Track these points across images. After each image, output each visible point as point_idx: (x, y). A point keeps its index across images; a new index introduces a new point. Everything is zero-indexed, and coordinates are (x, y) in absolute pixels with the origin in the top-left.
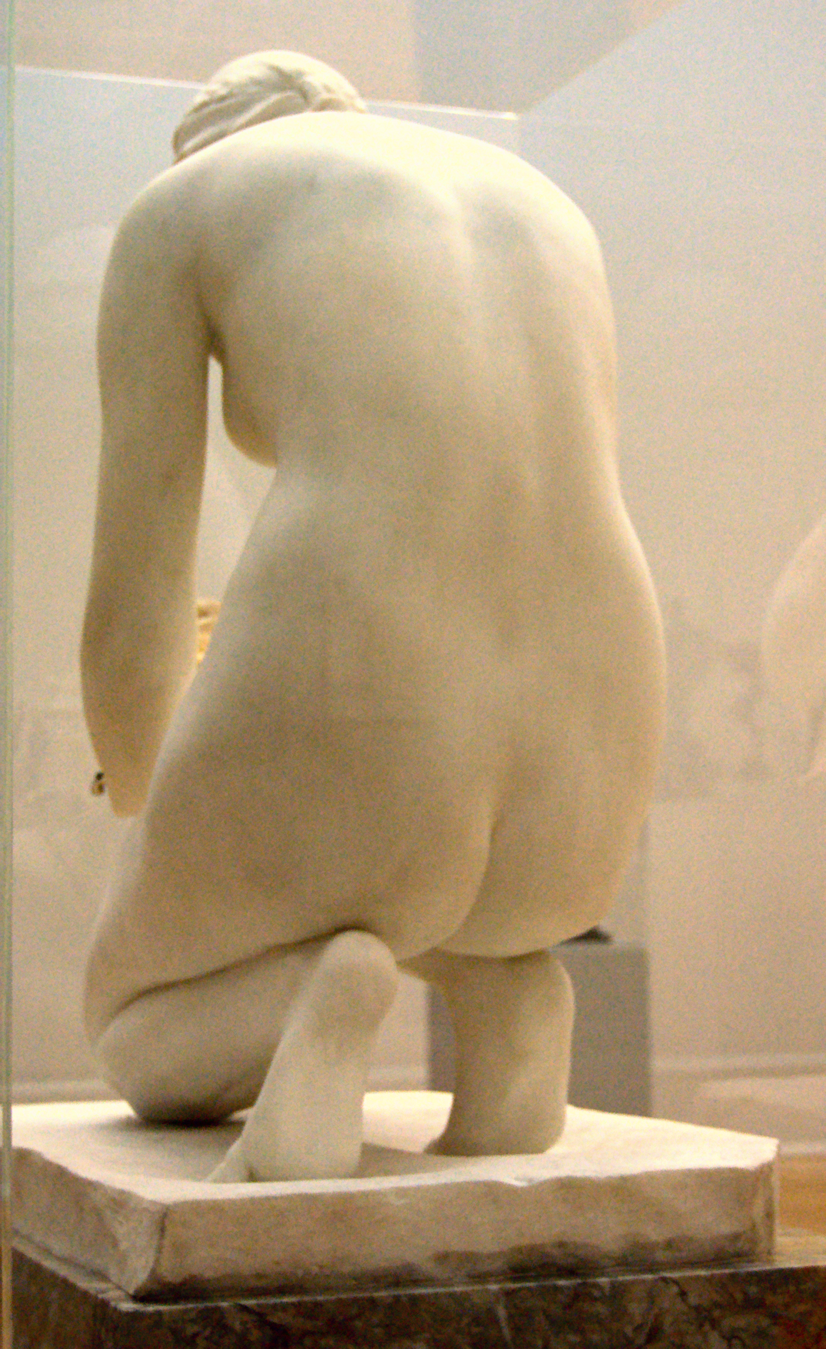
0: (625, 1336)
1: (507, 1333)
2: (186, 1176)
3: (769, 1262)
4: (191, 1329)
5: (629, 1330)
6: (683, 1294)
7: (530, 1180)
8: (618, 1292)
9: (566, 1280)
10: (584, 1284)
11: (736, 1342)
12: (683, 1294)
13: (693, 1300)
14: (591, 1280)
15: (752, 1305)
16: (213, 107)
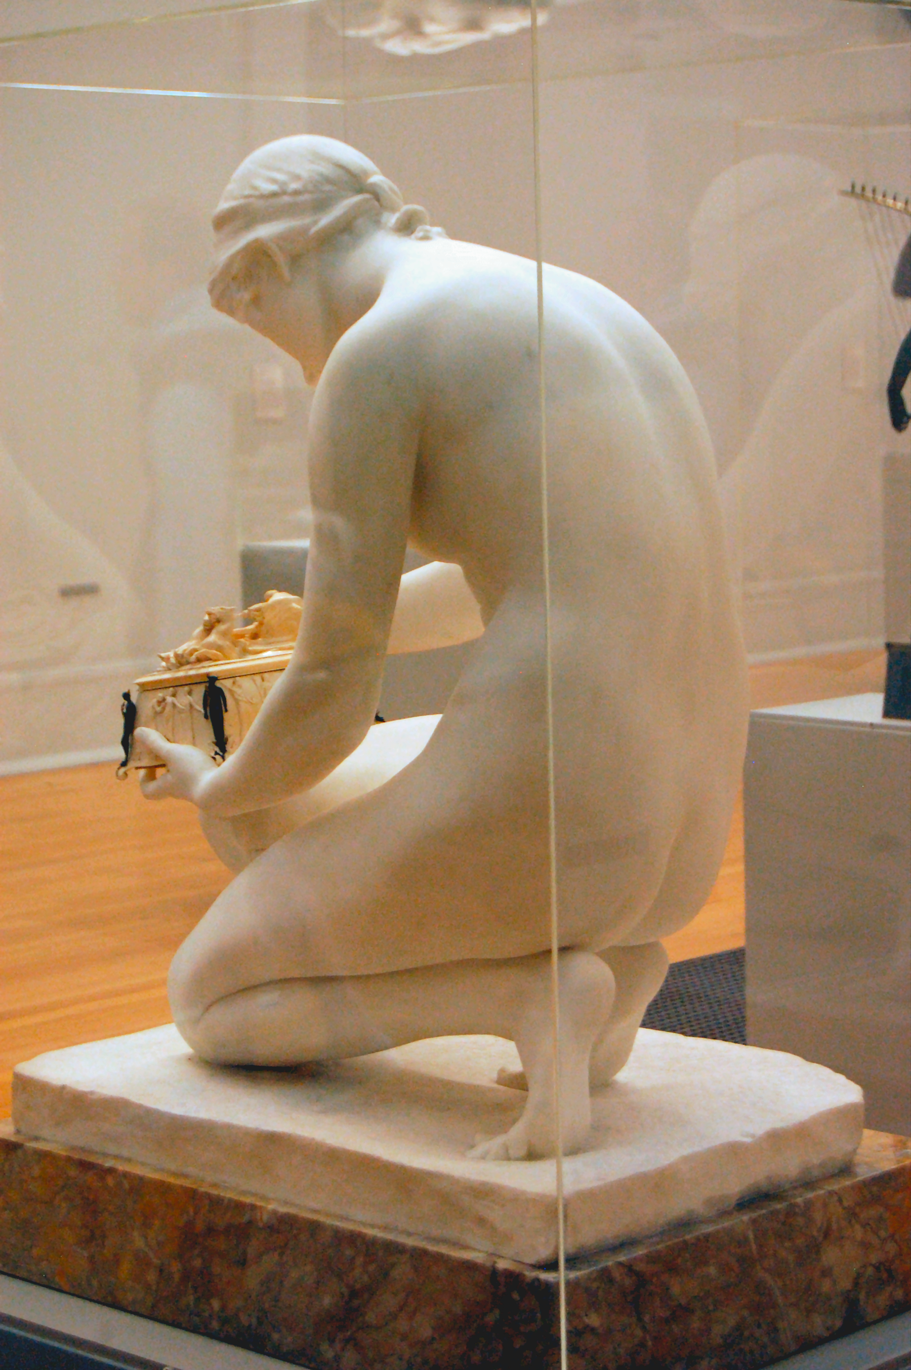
0: (813, 1237)
2: (211, 673)
3: (856, 1175)
4: (595, 1285)
6: (840, 1201)
7: (753, 1136)
9: (859, 1180)
10: (791, 1204)
11: (868, 1228)
12: (840, 1201)
14: (793, 1201)
15: (876, 1200)
16: (286, 199)
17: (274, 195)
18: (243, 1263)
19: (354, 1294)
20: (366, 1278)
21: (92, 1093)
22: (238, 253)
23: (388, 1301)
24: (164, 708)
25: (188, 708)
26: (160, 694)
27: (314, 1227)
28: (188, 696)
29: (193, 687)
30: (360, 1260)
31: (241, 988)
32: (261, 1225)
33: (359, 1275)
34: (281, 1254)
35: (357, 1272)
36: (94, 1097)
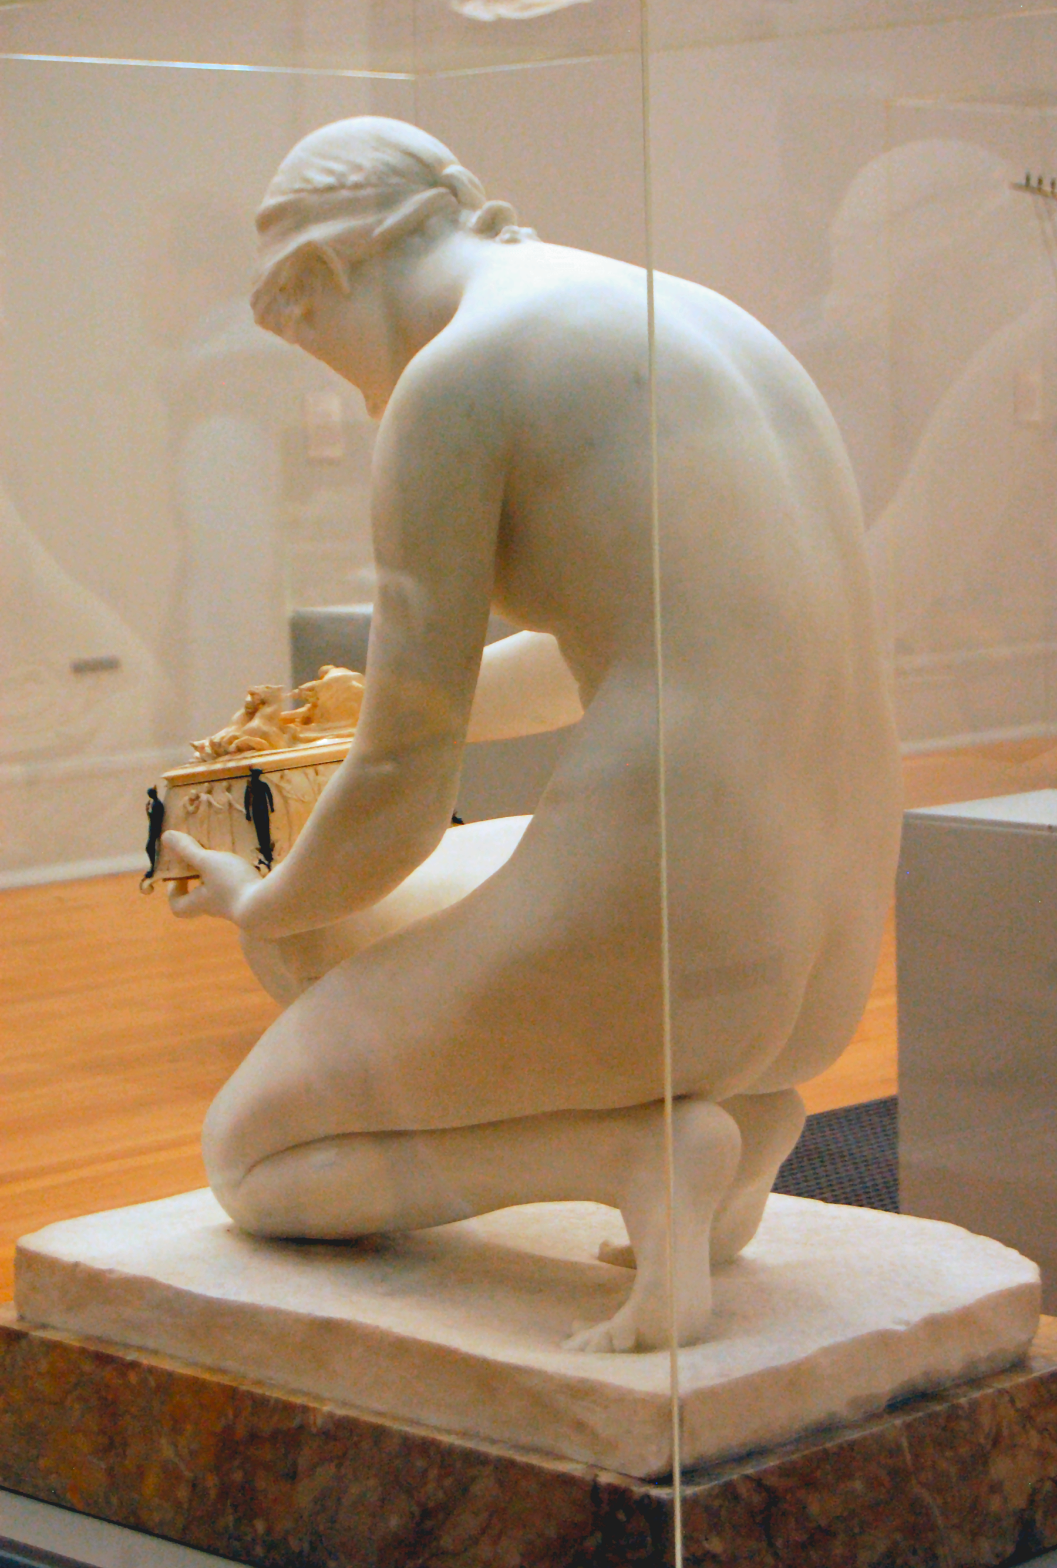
1: (908, 1457)
4: (717, 1503)
5: (982, 1440)
6: (1012, 1401)
7: (907, 1323)
8: (974, 1405)
10: (953, 1405)
11: (1046, 1434)
12: (1012, 1401)
13: (1019, 1405)
14: (955, 1402)
16: (345, 194)
17: (330, 188)
18: (292, 1476)
19: (426, 1513)
20: (441, 1495)
21: (111, 1271)
22: (287, 258)
23: (468, 1522)
24: (197, 808)
25: (227, 807)
26: (193, 791)
27: (379, 1433)
28: (227, 793)
29: (233, 782)
30: (433, 1473)
31: (291, 1145)
32: (314, 1430)
33: (432, 1491)
34: (339, 1466)
35: (431, 1487)
36: (113, 1276)
